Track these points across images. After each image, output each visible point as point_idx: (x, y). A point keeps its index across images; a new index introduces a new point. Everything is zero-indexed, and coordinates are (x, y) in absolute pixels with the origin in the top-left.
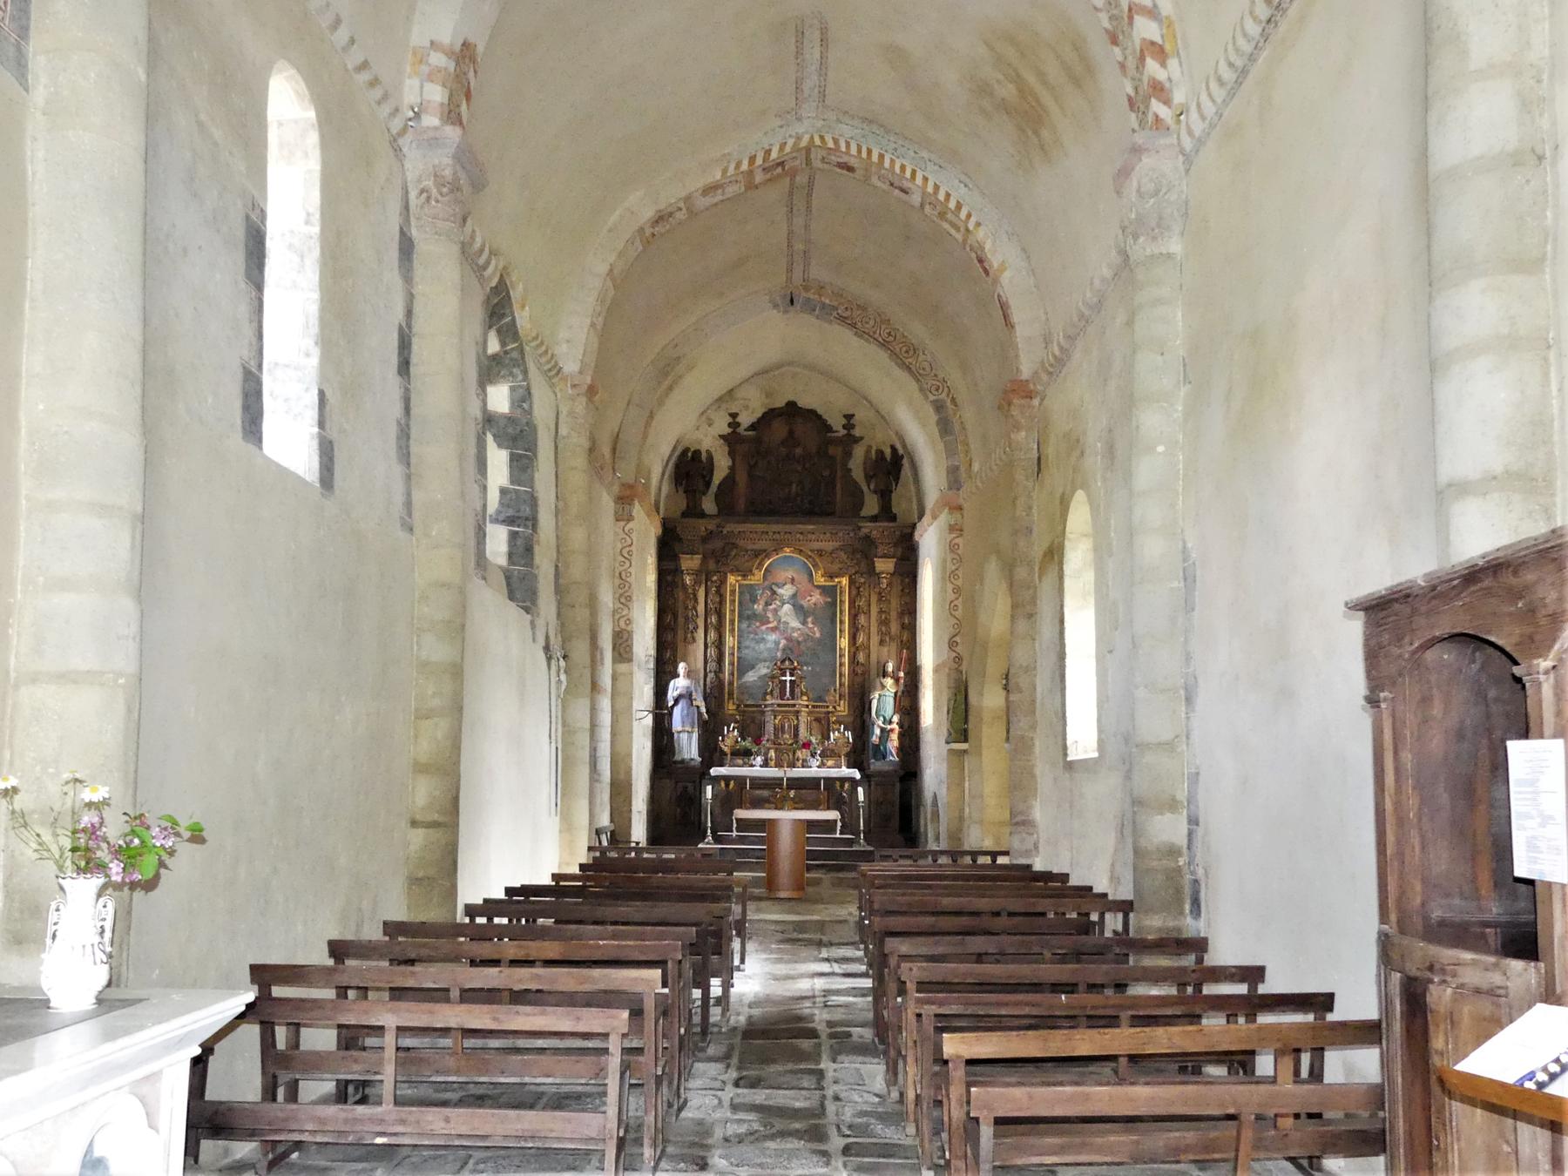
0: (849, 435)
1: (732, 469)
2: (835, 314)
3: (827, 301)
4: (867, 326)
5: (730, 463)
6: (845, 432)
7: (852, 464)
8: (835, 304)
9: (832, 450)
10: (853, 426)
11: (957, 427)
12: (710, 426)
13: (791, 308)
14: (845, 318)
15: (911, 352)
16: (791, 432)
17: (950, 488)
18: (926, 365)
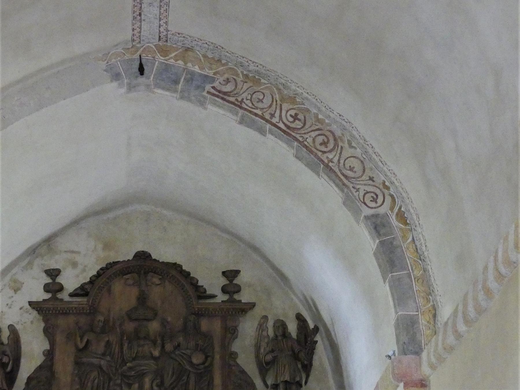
0: (232, 301)
1: (49, 354)
2: (208, 87)
3: (197, 69)
4: (260, 105)
5: (47, 347)
6: (226, 297)
7: (236, 347)
8: (210, 73)
9: (205, 325)
10: (238, 289)
11: (409, 255)
12: (16, 291)
13: (141, 80)
14: (225, 93)
15: (331, 145)
16: (142, 299)
17: (404, 352)
18: (355, 163)
